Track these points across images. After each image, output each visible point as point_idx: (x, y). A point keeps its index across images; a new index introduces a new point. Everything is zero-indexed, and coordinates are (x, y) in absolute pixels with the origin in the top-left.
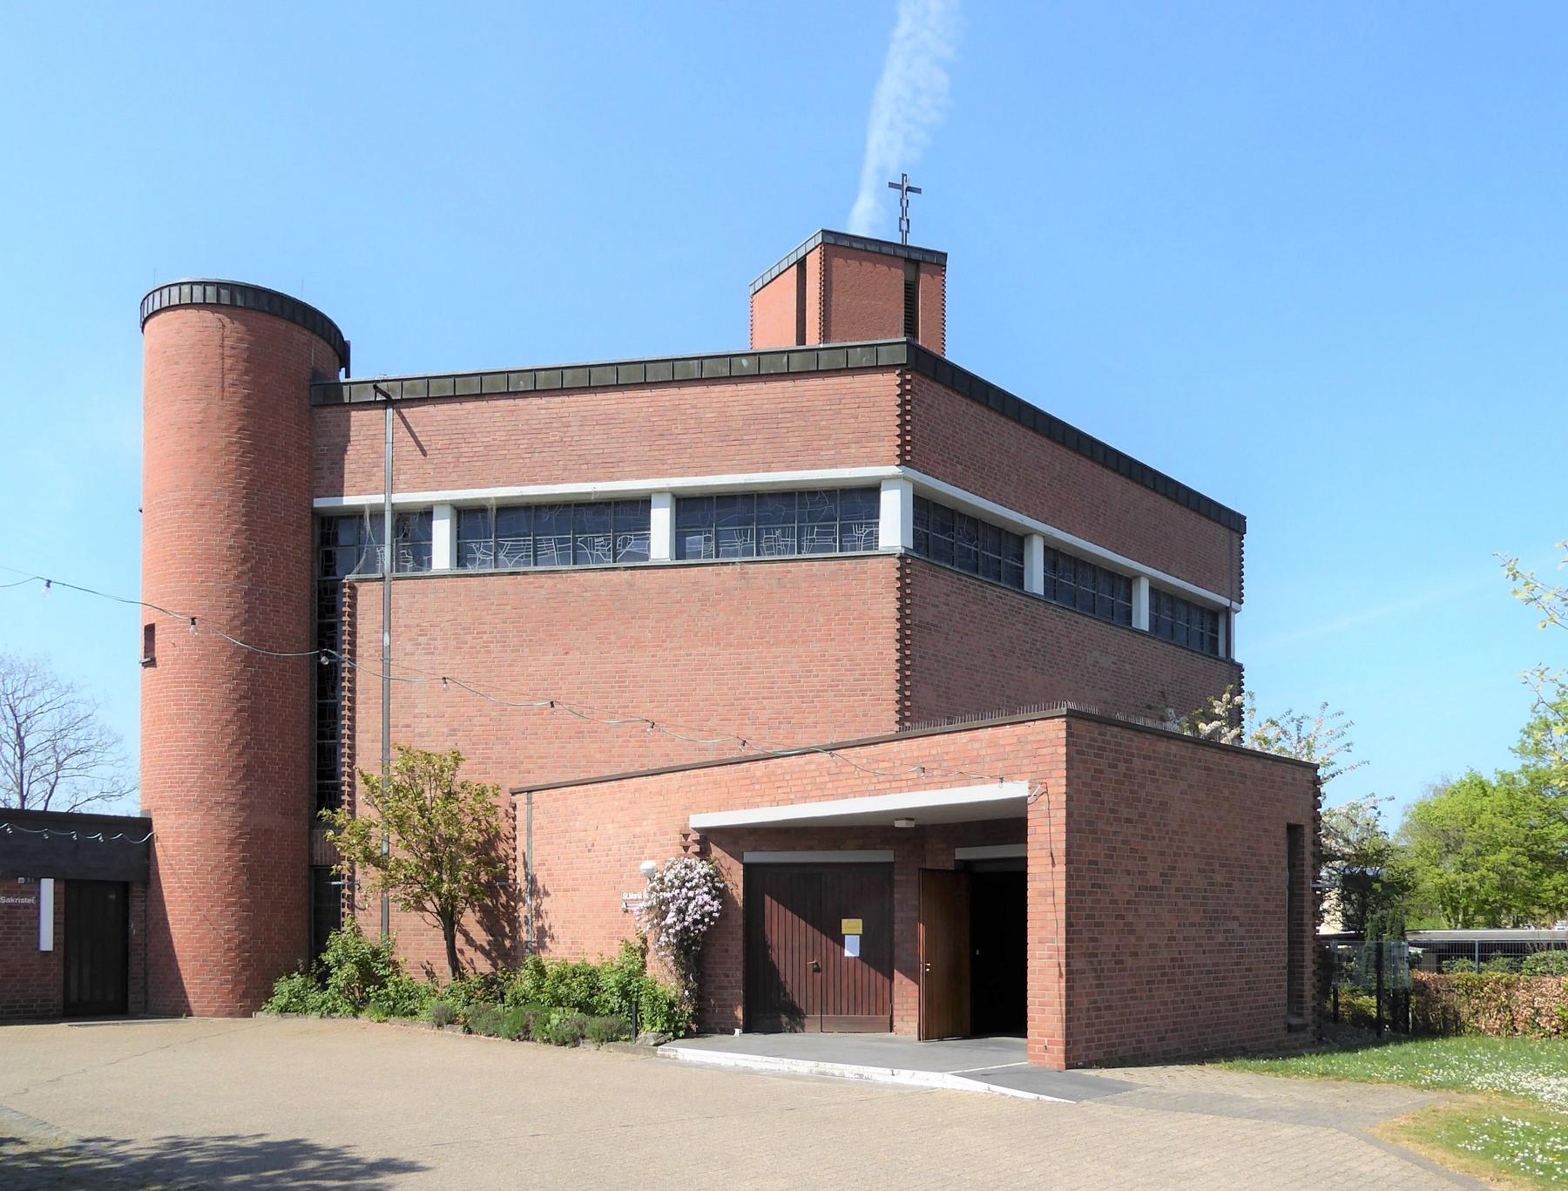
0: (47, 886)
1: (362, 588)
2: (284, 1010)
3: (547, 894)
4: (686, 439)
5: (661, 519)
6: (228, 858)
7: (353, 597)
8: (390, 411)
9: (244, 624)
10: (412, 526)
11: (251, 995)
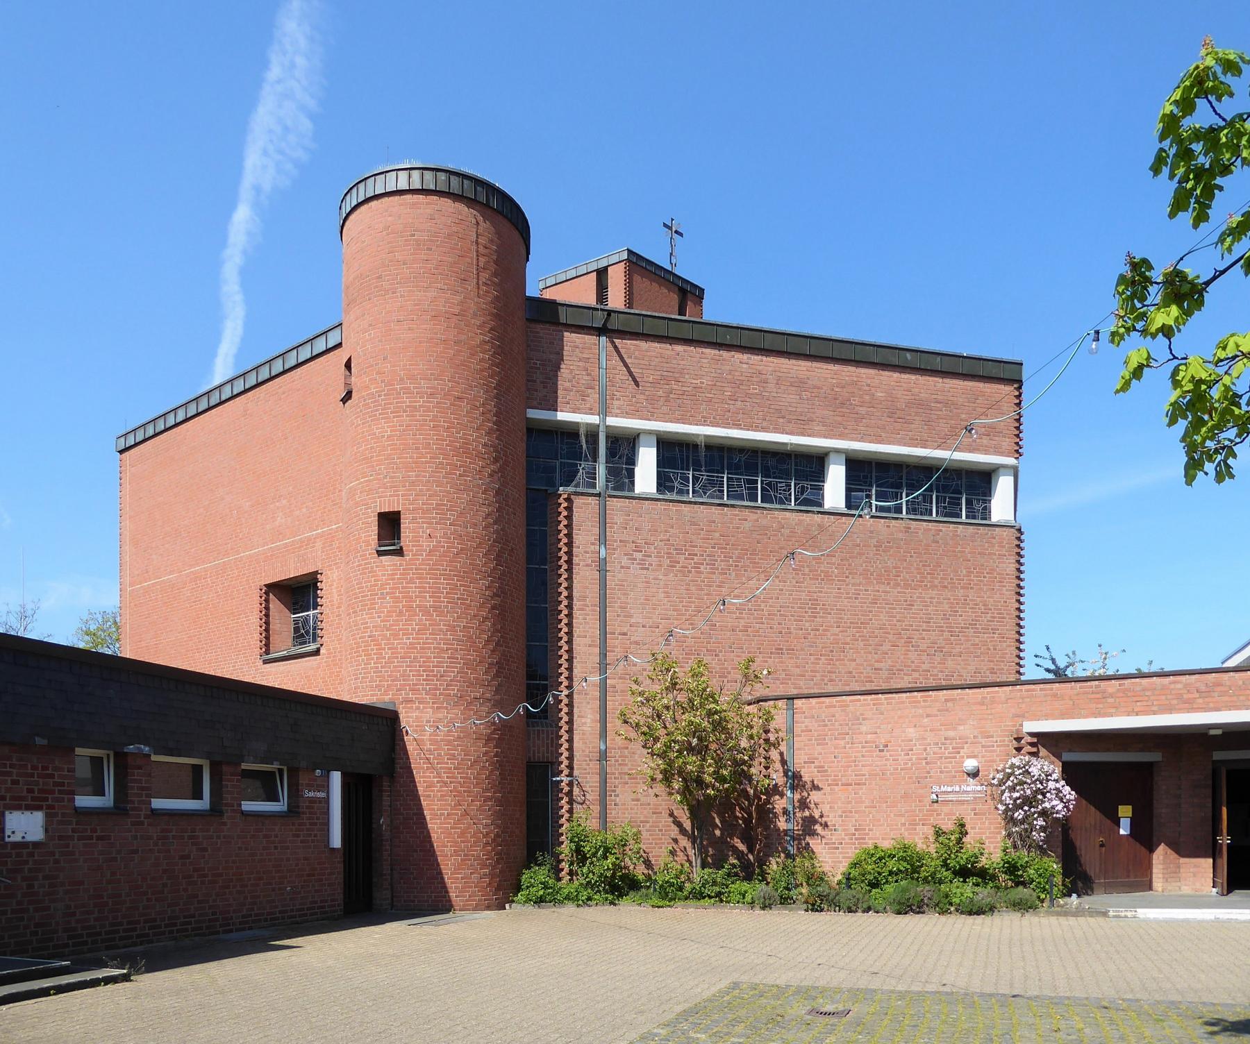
0: (336, 778)
1: (578, 502)
2: (540, 901)
3: (816, 788)
4: (863, 410)
5: (836, 477)
6: (485, 754)
7: (569, 509)
8: (603, 339)
9: (495, 523)
10: (623, 448)
11: (504, 889)
